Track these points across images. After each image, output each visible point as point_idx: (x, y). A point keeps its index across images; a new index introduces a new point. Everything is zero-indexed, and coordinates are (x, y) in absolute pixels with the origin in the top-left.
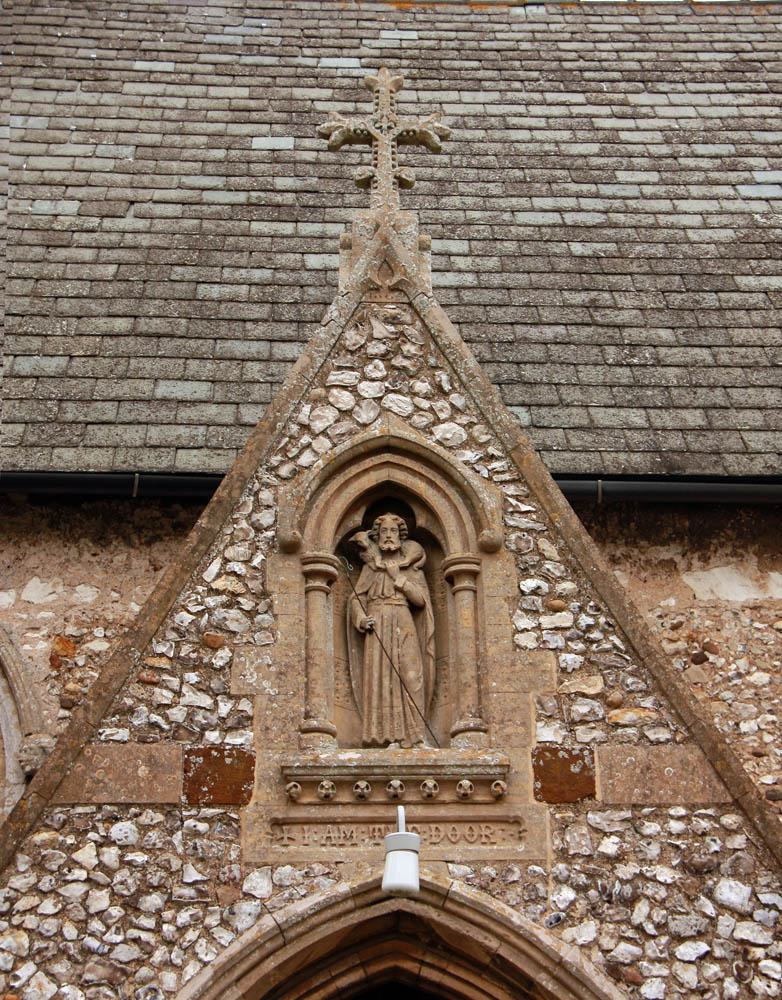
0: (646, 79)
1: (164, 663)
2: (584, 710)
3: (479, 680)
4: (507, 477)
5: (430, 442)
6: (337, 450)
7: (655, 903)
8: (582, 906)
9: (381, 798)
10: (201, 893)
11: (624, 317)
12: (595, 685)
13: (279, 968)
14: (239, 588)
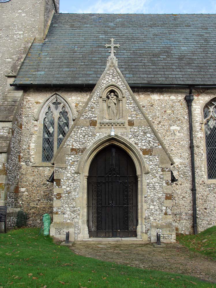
0: (151, 26)
1: (87, 110)
2: (134, 116)
3: (122, 112)
4: (126, 89)
5: (117, 85)
6: (106, 86)
7: (140, 136)
8: (132, 137)
9: (111, 125)
10: (92, 135)
11: (145, 62)
12: (135, 113)
13: (100, 143)
14: (95, 102)
